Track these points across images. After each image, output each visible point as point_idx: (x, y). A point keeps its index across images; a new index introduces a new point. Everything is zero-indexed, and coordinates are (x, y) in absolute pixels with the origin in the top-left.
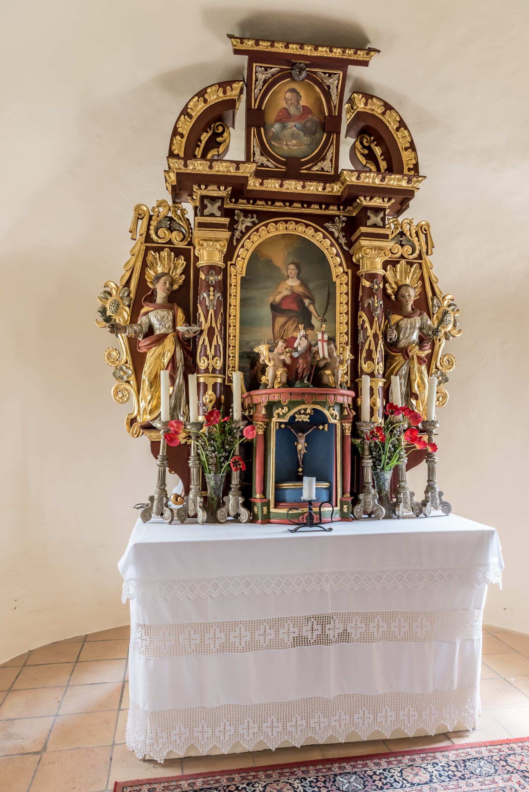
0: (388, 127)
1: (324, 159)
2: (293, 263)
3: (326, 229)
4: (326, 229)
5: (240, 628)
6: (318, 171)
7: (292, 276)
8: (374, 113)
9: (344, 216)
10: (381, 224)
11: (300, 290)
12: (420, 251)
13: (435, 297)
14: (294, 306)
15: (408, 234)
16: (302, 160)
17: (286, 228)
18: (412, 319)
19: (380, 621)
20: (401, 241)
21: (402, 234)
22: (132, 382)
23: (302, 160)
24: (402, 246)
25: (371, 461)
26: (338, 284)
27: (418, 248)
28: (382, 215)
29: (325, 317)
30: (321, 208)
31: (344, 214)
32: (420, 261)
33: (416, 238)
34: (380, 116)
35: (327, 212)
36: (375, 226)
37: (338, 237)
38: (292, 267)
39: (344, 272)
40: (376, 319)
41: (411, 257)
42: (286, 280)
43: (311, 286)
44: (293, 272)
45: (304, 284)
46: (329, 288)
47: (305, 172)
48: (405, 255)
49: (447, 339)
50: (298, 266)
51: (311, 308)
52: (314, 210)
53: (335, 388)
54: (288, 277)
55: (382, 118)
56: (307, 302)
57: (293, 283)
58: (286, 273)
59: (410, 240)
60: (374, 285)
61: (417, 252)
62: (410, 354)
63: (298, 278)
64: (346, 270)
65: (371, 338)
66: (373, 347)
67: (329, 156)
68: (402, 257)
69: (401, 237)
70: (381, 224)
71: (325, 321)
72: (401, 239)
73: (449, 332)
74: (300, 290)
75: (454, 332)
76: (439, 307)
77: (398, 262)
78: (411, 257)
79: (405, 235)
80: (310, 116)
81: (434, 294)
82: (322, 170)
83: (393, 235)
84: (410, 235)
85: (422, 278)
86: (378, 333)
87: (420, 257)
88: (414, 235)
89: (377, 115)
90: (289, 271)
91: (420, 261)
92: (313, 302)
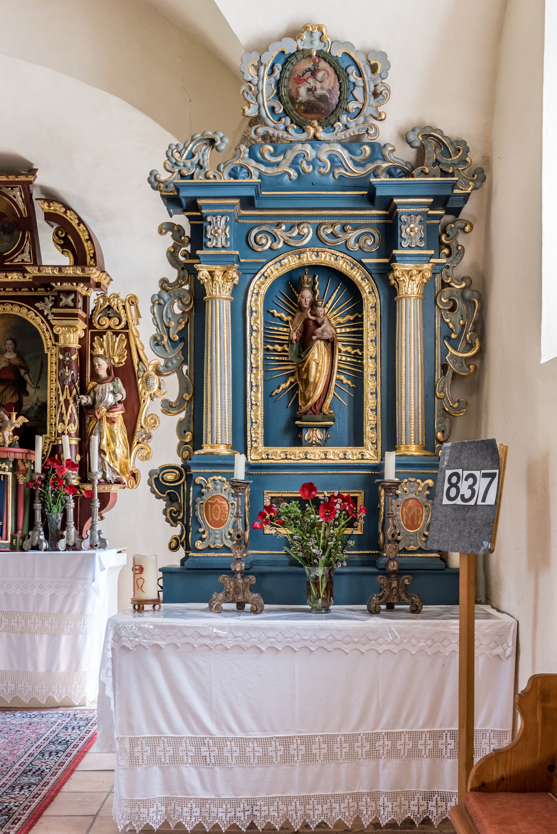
0: (71, 223)
1: (23, 252)
2: (11, 339)
3: (37, 309)
4: (37, 309)
5: (418, 813)
6: (19, 262)
7: (9, 350)
8: (57, 212)
9: (52, 296)
10: (72, 304)
11: (17, 362)
12: (127, 322)
13: (141, 363)
14: (11, 376)
15: (115, 308)
16: (5, 254)
17: (4, 309)
18: (104, 385)
19: (16, 627)
20: (109, 314)
21: (109, 307)
22: (139, 426)
23: (5, 254)
24: (110, 318)
25: (40, 505)
26: (49, 356)
27: (124, 320)
28: (72, 296)
29: (38, 384)
30: (30, 290)
31: (53, 294)
32: (127, 331)
33: (123, 310)
34: (63, 215)
35: (36, 294)
36: (66, 306)
37: (48, 315)
38: (9, 342)
39: (53, 345)
40: (67, 386)
41: (118, 328)
42: (4, 354)
43: (26, 358)
44: (10, 346)
45: (20, 356)
46: (42, 359)
47: (8, 263)
48: (113, 326)
49: (152, 399)
50: (14, 341)
51: (26, 377)
52: (25, 292)
53: (3, 446)
54: (6, 351)
55: (65, 216)
56: (22, 372)
57: (10, 356)
58: (4, 347)
59: (116, 312)
60: (65, 357)
61: (123, 323)
62: (98, 417)
63: (15, 351)
64: (54, 343)
65: (62, 403)
66: (64, 410)
67: (27, 249)
68: (109, 328)
69: (108, 310)
70: (72, 304)
71: (39, 388)
72: (108, 312)
73: (154, 394)
74: (17, 362)
75: (157, 394)
76: (144, 371)
77: (105, 333)
78: (118, 328)
79: (112, 308)
80: (6, 219)
81: (140, 360)
82: (23, 261)
83: (102, 309)
84: (117, 308)
85: (128, 347)
86: (69, 398)
87: (127, 327)
88: (121, 308)
89: (60, 214)
90: (6, 346)
91: (127, 331)
92: (28, 372)
